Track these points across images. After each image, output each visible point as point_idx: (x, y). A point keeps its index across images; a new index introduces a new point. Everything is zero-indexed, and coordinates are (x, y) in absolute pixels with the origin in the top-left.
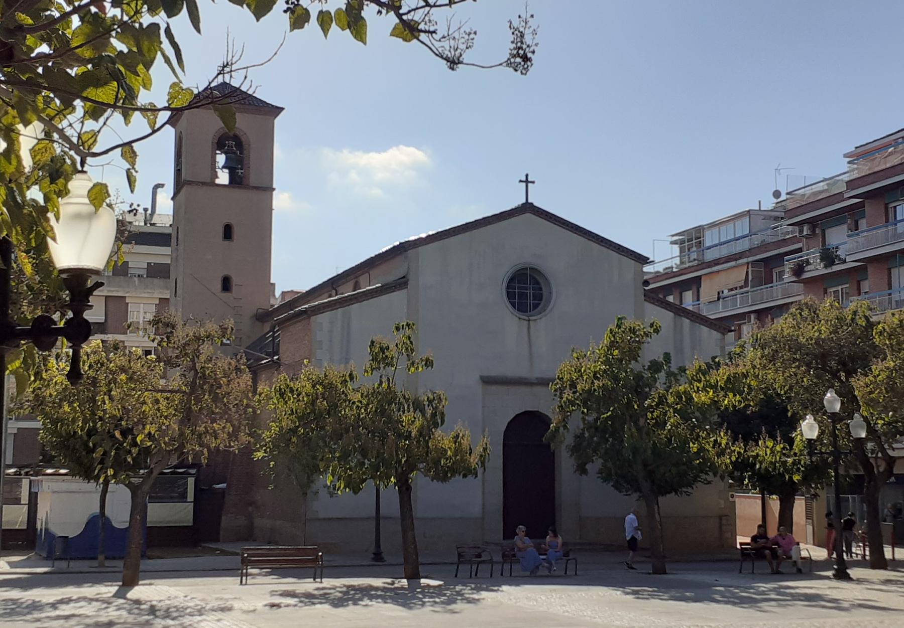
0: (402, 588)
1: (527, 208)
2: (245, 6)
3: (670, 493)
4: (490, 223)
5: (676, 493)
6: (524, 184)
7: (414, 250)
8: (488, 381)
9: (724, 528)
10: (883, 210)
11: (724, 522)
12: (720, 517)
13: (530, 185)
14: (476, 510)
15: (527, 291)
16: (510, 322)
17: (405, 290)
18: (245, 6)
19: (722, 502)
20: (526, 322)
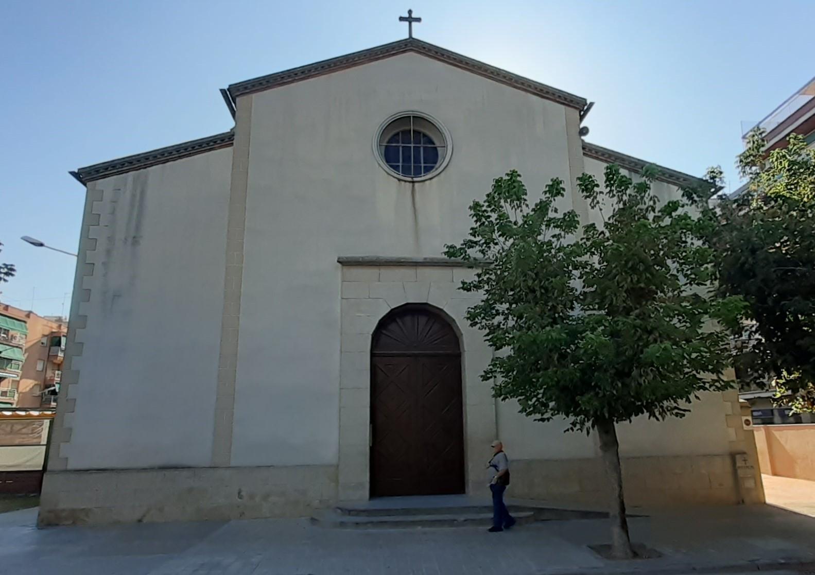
0: (783, 224)
1: (411, 45)
2: (729, 388)
3: (638, 411)
4: (355, 65)
5: (652, 414)
6: (407, 23)
7: (245, 97)
8: (345, 263)
9: (741, 473)
10: (508, 458)
11: (739, 463)
12: (733, 456)
13: (414, 24)
14: (329, 455)
15: (411, 147)
16: (387, 186)
17: (229, 150)
18: (729, 388)
19: (732, 431)
20: (409, 185)
